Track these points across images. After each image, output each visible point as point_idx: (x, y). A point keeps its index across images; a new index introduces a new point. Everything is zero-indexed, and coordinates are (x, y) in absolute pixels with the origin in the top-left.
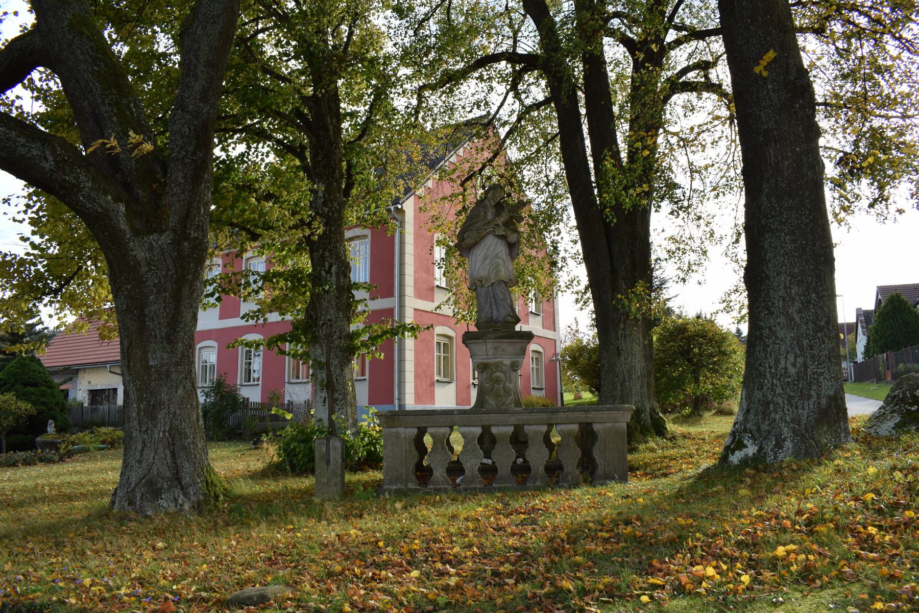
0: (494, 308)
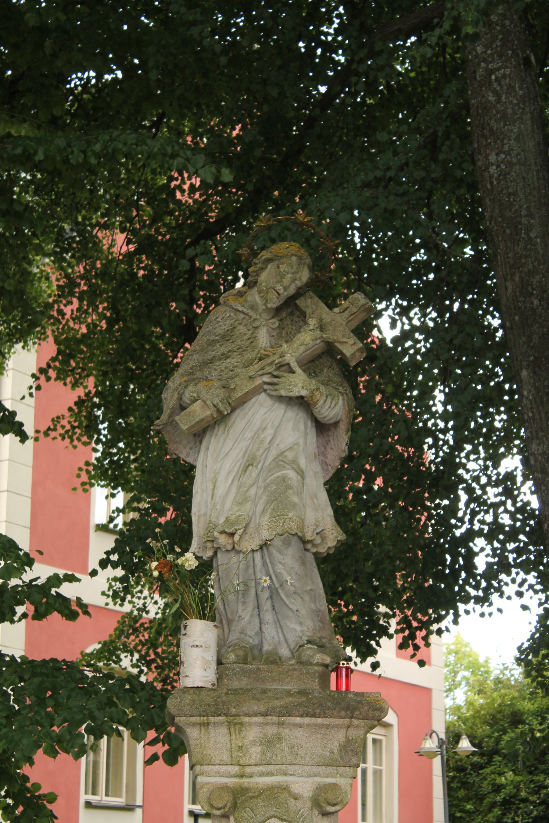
0: (269, 617)
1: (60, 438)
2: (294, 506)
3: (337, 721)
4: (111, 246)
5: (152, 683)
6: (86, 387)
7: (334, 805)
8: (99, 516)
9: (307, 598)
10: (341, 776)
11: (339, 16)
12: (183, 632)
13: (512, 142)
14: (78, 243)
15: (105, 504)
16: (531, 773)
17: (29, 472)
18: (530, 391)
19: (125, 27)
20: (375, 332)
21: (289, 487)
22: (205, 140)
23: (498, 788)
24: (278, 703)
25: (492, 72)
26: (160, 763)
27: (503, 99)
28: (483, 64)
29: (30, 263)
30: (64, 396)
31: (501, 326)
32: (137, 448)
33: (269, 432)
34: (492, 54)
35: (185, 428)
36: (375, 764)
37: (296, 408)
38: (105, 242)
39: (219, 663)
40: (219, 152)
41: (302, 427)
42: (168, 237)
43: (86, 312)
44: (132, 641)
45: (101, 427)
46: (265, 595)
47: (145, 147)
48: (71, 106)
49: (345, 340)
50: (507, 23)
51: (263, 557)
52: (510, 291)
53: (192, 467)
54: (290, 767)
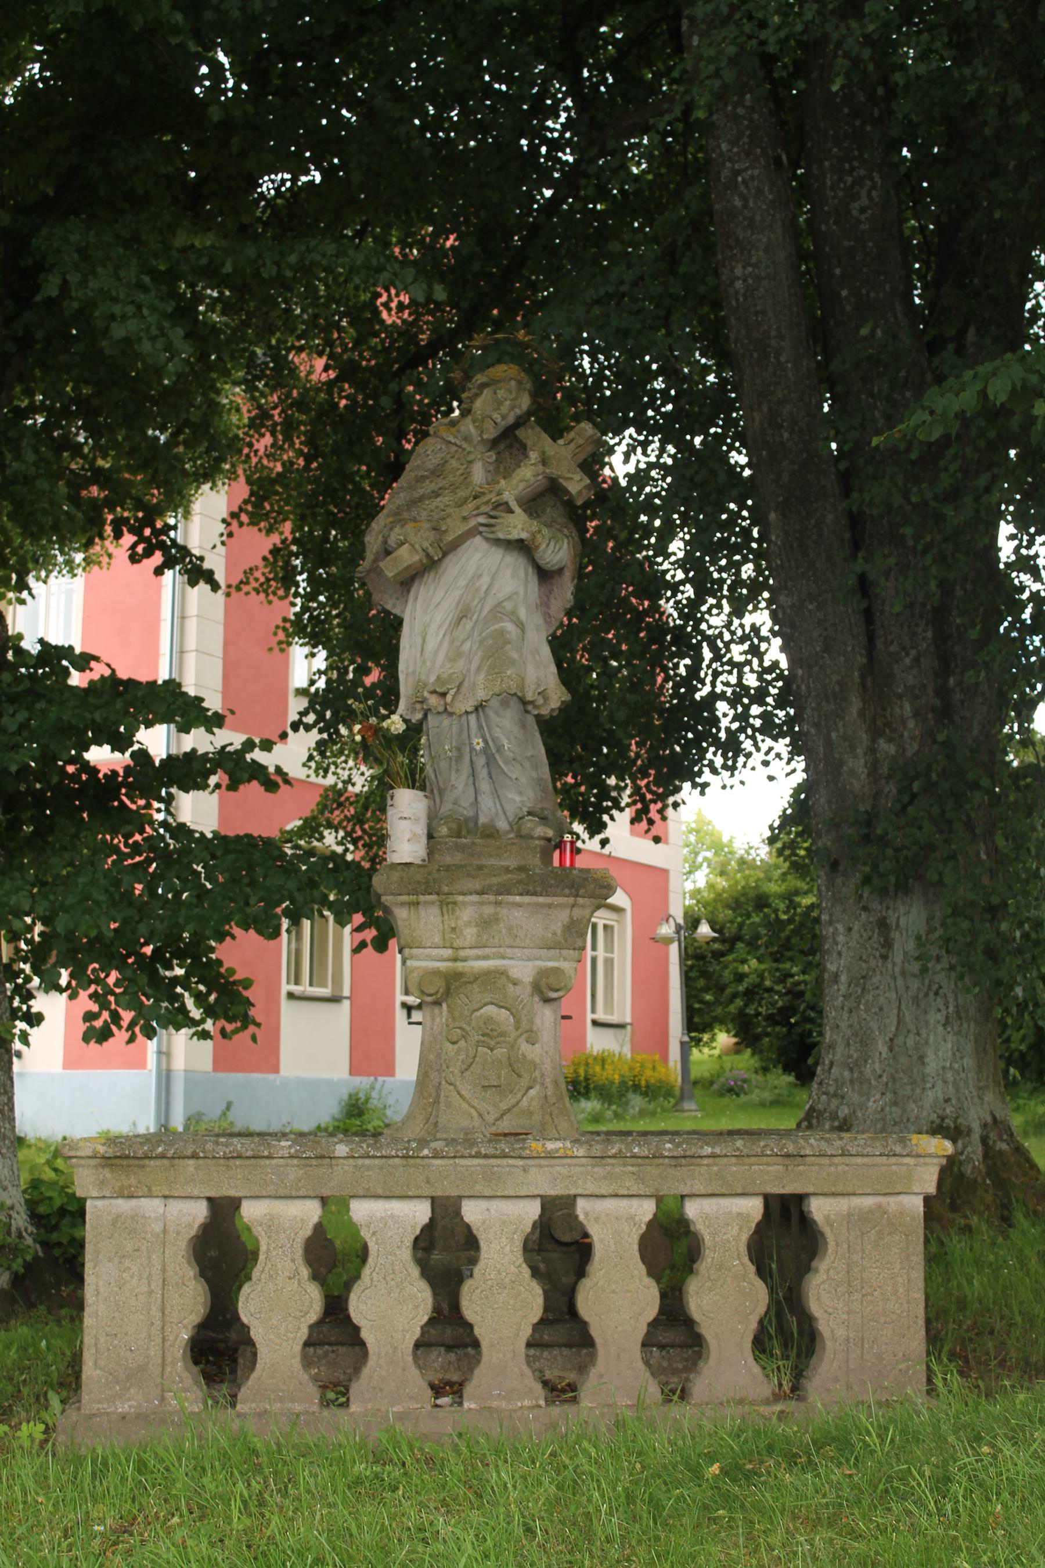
0: (485, 786)
1: (253, 594)
2: (513, 662)
3: (561, 900)
4: (309, 373)
5: (359, 863)
6: (281, 533)
7: (557, 990)
8: (299, 677)
9: (527, 765)
10: (565, 959)
11: (567, 109)
12: (389, 802)
13: (761, 253)
14: (272, 369)
15: (305, 666)
16: (776, 961)
17: (220, 629)
18: (778, 536)
19: (324, 122)
20: (607, 471)
21: (508, 642)
22: (415, 252)
23: (740, 977)
24: (494, 880)
25: (738, 172)
26: (369, 950)
27: (751, 204)
28: (728, 164)
29: (218, 392)
30: (259, 544)
31: (749, 465)
32: (340, 601)
33: (485, 580)
34: (738, 153)
35: (390, 575)
36: (606, 951)
37: (515, 553)
38: (302, 368)
39: (430, 836)
40: (431, 267)
41: (522, 574)
42: (373, 363)
43: (281, 448)
44: (337, 816)
45: (299, 578)
46: (481, 761)
47: (347, 260)
48: (263, 212)
49: (569, 475)
50: (756, 116)
51: (478, 720)
52: (757, 422)
53: (399, 622)
54: (508, 950)
